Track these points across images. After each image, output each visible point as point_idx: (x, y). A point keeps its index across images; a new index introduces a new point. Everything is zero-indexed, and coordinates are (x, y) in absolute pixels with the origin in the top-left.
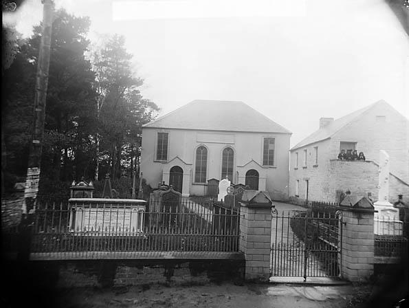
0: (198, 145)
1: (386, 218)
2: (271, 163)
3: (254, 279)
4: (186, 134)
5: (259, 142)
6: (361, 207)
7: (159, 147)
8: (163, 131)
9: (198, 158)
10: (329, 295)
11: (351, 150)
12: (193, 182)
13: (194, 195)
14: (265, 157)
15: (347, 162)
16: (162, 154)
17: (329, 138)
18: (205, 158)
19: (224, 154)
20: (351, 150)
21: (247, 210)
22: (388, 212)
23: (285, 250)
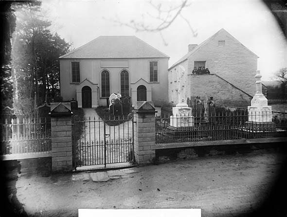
0: (102, 70)
1: (183, 115)
2: (156, 80)
3: (60, 170)
4: (93, 63)
5: (146, 65)
6: (145, 110)
7: (73, 72)
8: (75, 61)
9: (103, 79)
10: (247, 168)
11: (201, 67)
12: (101, 96)
13: (102, 106)
14: (151, 76)
15: (198, 76)
16: (76, 77)
17: (187, 59)
18: (108, 79)
19: (121, 76)
20: (201, 67)
21: (137, 115)
22: (184, 111)
23: (97, 146)
